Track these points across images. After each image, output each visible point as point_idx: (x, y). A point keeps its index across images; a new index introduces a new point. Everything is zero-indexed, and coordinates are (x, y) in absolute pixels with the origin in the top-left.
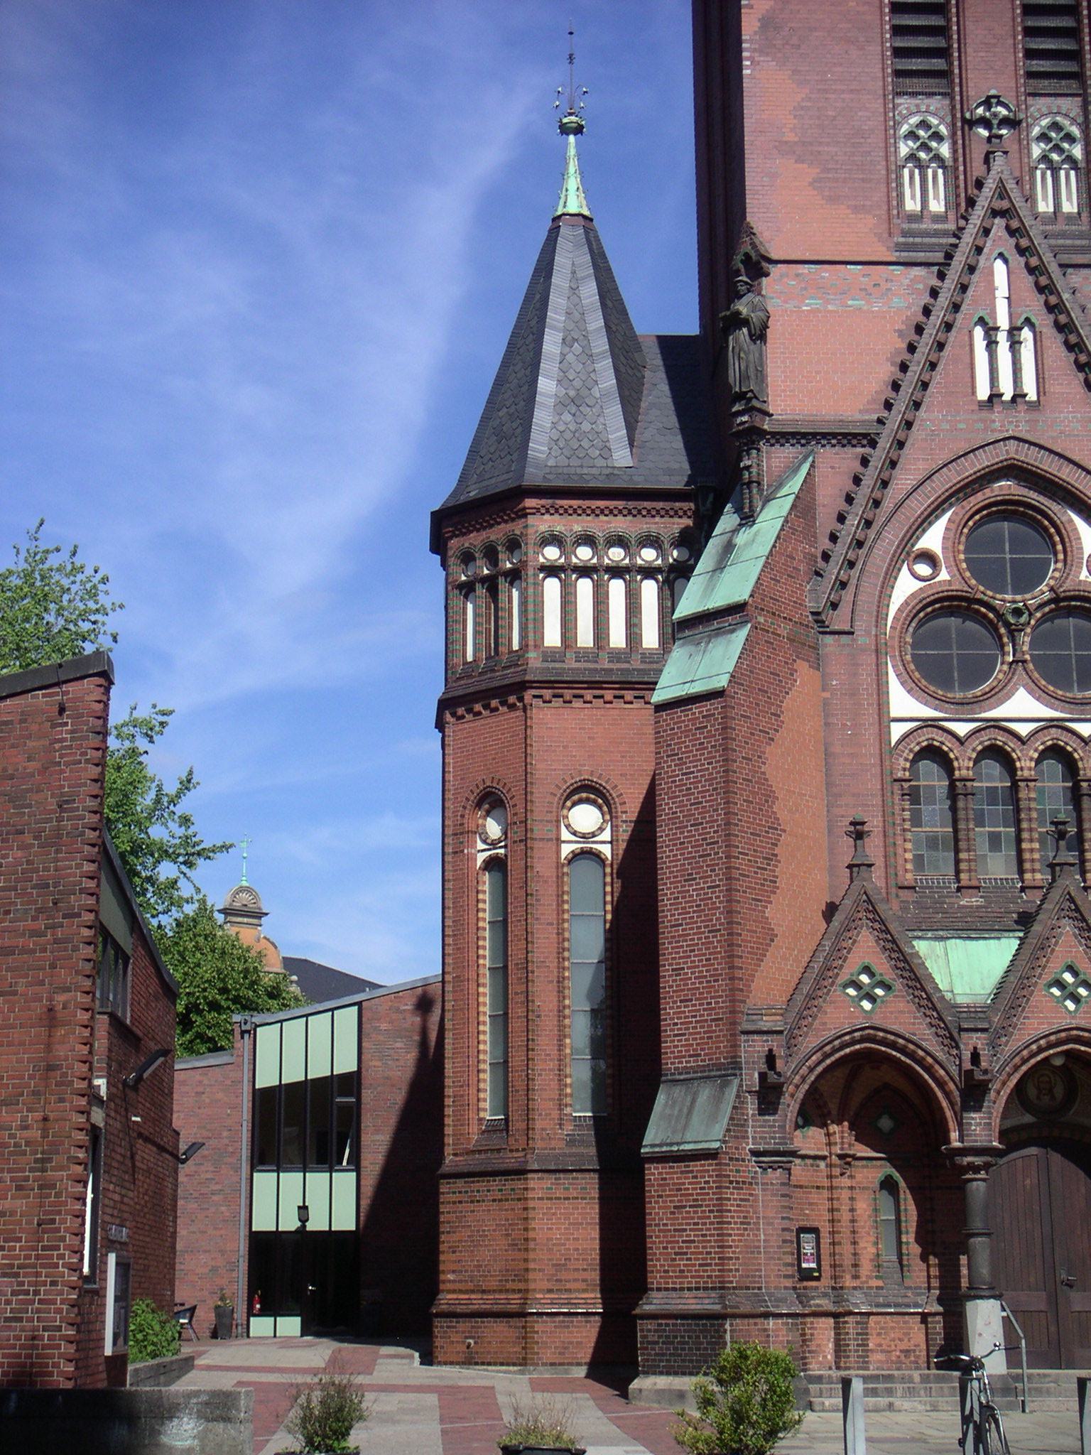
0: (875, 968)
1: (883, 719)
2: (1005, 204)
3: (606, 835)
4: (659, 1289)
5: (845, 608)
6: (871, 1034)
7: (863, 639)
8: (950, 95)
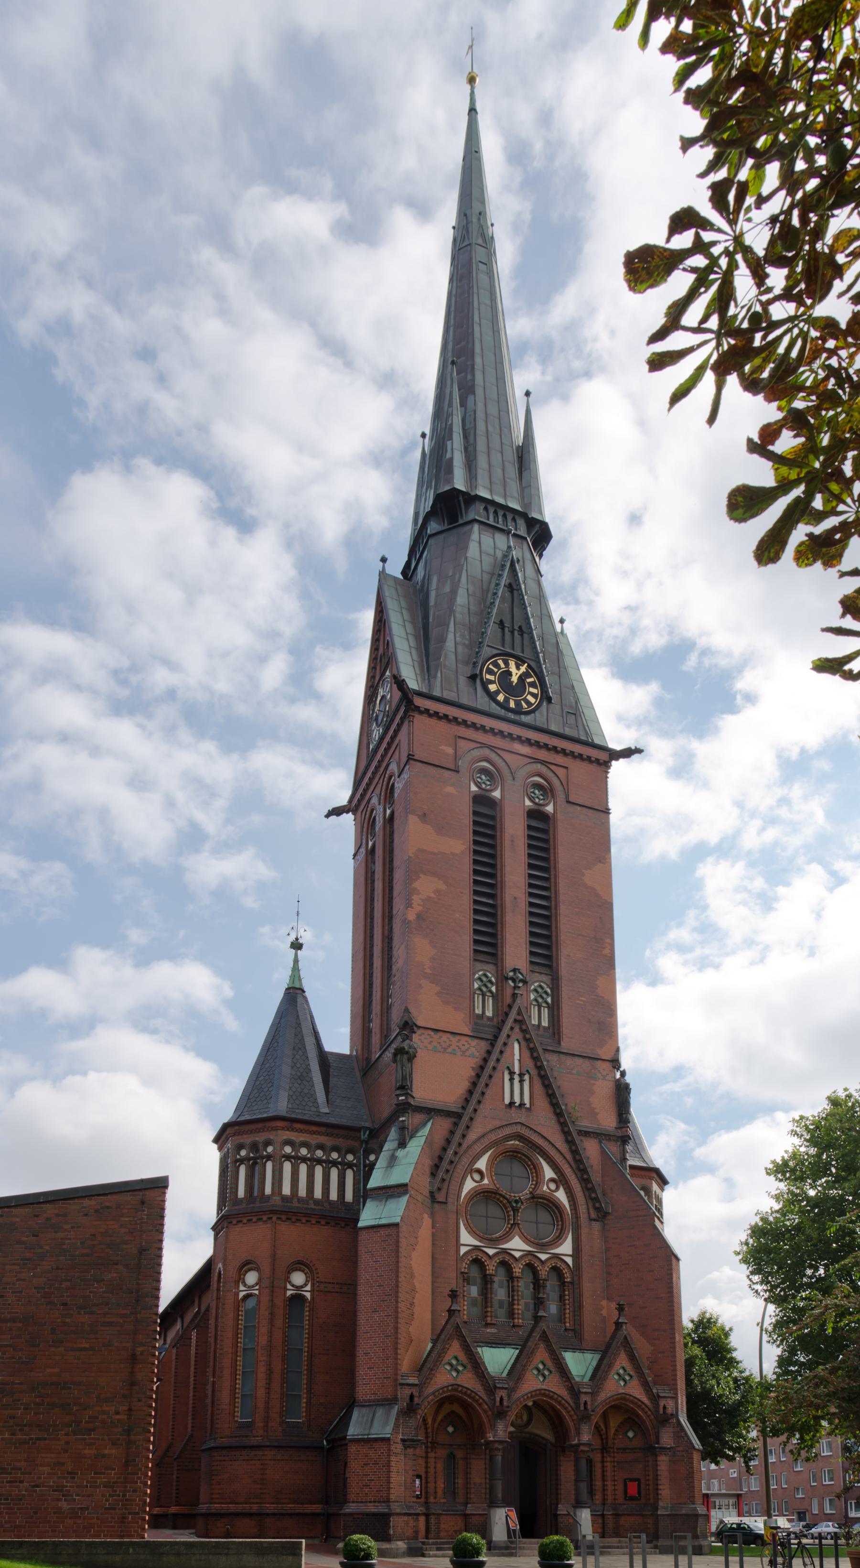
0: (460, 1358)
1: (458, 1245)
2: (519, 1018)
3: (308, 1288)
4: (353, 1502)
5: (444, 1192)
6: (455, 1387)
7: (451, 1207)
8: (496, 965)
